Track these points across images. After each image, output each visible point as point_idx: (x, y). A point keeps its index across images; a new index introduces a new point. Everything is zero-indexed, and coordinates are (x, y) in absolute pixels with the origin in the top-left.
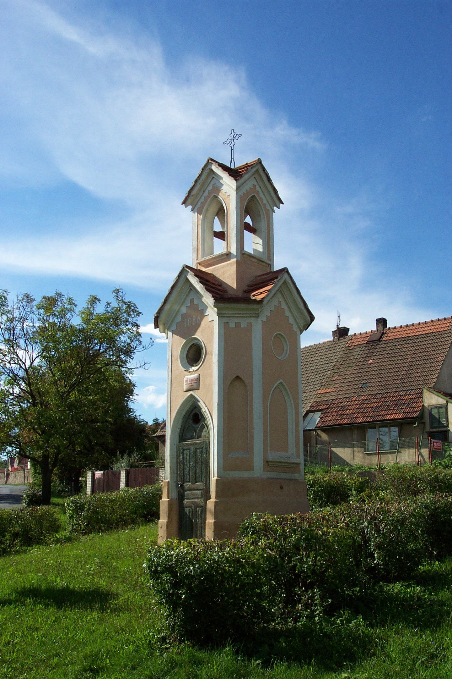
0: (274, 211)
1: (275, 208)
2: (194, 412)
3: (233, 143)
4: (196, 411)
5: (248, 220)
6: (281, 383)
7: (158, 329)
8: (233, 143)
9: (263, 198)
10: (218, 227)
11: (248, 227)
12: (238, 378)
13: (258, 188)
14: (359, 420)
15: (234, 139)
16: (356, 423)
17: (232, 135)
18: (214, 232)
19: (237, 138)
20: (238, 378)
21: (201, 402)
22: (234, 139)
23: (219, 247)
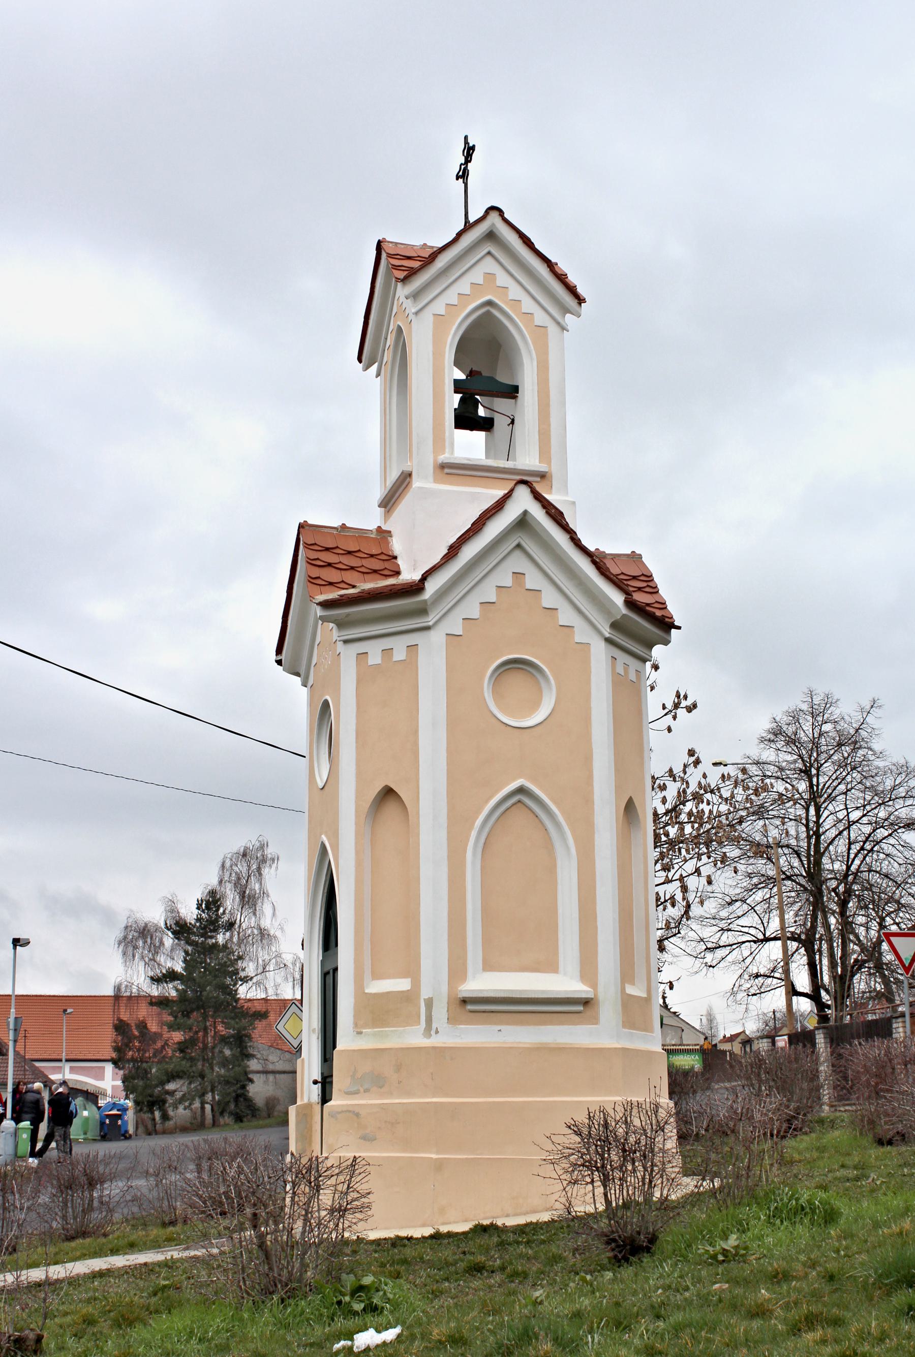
6: (521, 790)
9: (521, 304)
12: (388, 793)
20: (388, 793)
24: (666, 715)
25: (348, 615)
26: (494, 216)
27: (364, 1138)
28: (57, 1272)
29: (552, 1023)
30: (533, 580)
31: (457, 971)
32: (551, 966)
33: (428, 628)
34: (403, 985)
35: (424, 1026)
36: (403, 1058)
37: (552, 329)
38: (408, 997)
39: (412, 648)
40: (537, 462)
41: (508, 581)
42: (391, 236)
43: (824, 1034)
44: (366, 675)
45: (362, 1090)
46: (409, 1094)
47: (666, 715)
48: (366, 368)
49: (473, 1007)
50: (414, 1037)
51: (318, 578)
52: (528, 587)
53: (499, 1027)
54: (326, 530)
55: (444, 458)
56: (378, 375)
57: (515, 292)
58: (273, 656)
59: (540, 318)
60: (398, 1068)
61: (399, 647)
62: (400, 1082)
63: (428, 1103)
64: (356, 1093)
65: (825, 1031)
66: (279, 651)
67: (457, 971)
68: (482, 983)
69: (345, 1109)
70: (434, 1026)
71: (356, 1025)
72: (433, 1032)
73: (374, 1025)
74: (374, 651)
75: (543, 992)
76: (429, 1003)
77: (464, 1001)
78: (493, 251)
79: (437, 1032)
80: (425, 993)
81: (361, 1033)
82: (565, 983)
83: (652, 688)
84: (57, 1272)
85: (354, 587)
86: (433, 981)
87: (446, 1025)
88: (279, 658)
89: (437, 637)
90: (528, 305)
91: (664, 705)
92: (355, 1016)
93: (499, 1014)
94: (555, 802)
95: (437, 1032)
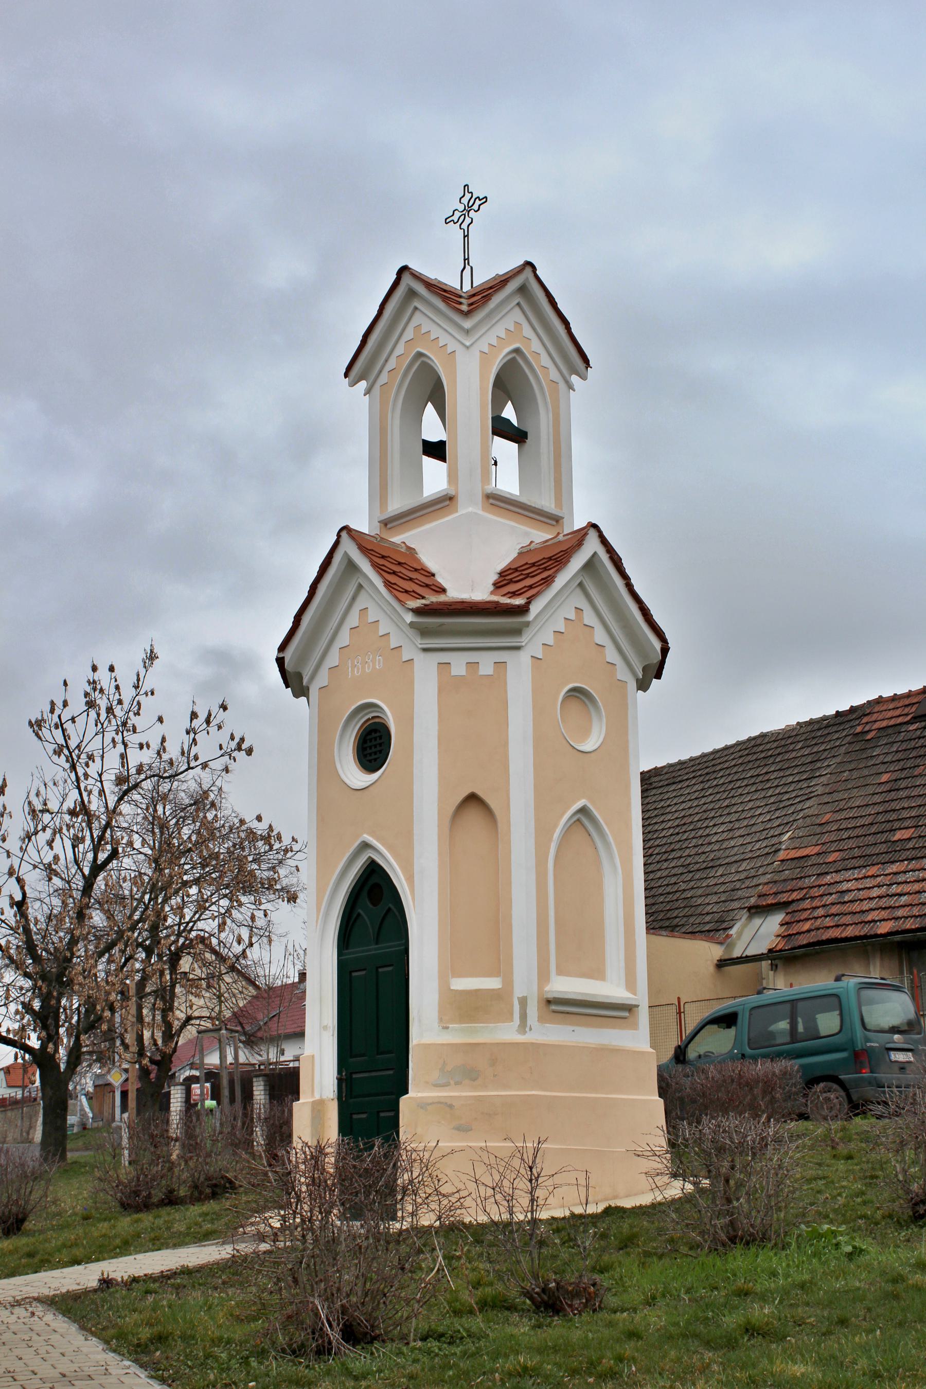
0: (570, 387)
1: (574, 379)
2: (370, 883)
3: (468, 220)
4: (374, 880)
5: (509, 413)
6: (583, 810)
7: (303, 699)
8: (468, 220)
9: (542, 360)
10: (432, 428)
11: (502, 429)
12: (473, 799)
13: (527, 331)
14: (883, 928)
15: (468, 209)
16: (876, 936)
17: (465, 200)
18: (424, 441)
19: (476, 207)
20: (473, 799)
21: (142, 1376)
22: (468, 209)
23: (435, 476)
24: (222, 756)
25: (443, 624)
26: (528, 270)
27: (458, 1129)
28: (122, 1268)
29: (607, 1027)
30: (589, 618)
31: (543, 976)
32: (598, 973)
33: (518, 648)
34: (492, 983)
35: (518, 1023)
36: (498, 1054)
37: (562, 385)
38: (500, 997)
39: (500, 665)
40: (553, 506)
41: (572, 616)
42: (414, 266)
43: (264, 1081)
44: (448, 686)
45: (452, 1082)
46: (506, 1087)
47: (222, 756)
48: (353, 384)
49: (560, 1007)
50: (506, 1033)
51: (395, 584)
52: (586, 623)
53: (572, 1028)
54: (368, 538)
55: (491, 488)
56: (368, 392)
57: (536, 345)
58: (275, 654)
59: (554, 374)
60: (493, 1062)
61: (486, 663)
62: (495, 1076)
63: (528, 1095)
64: (446, 1085)
65: (265, 1078)
66: (282, 648)
67: (543, 976)
68: (565, 986)
69: (430, 1101)
70: (529, 1023)
71: (441, 1020)
72: (527, 1029)
73: (461, 1022)
74: (459, 664)
75: (607, 997)
76: (523, 1002)
77: (549, 1002)
78: (522, 303)
79: (531, 1029)
80: (518, 992)
81: (447, 1028)
82: (612, 989)
83: (220, 727)
84: (122, 1268)
85: (423, 598)
86: (524, 982)
87: (537, 1023)
88: (281, 655)
89: (524, 657)
90: (545, 360)
91: (221, 745)
92: (439, 1012)
93: (578, 1017)
94: (606, 824)
95: (531, 1029)
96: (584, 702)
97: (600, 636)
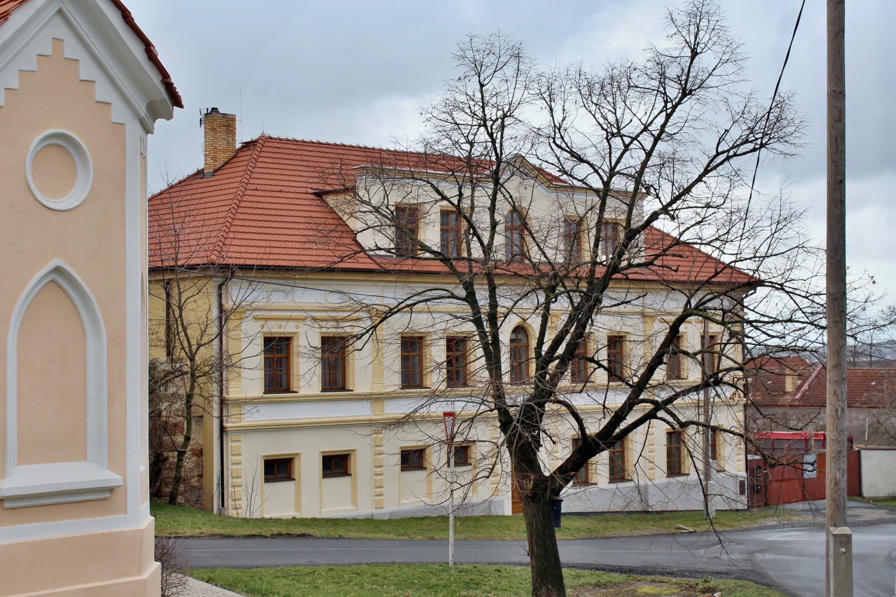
96: (69, 153)
97: (87, 70)
